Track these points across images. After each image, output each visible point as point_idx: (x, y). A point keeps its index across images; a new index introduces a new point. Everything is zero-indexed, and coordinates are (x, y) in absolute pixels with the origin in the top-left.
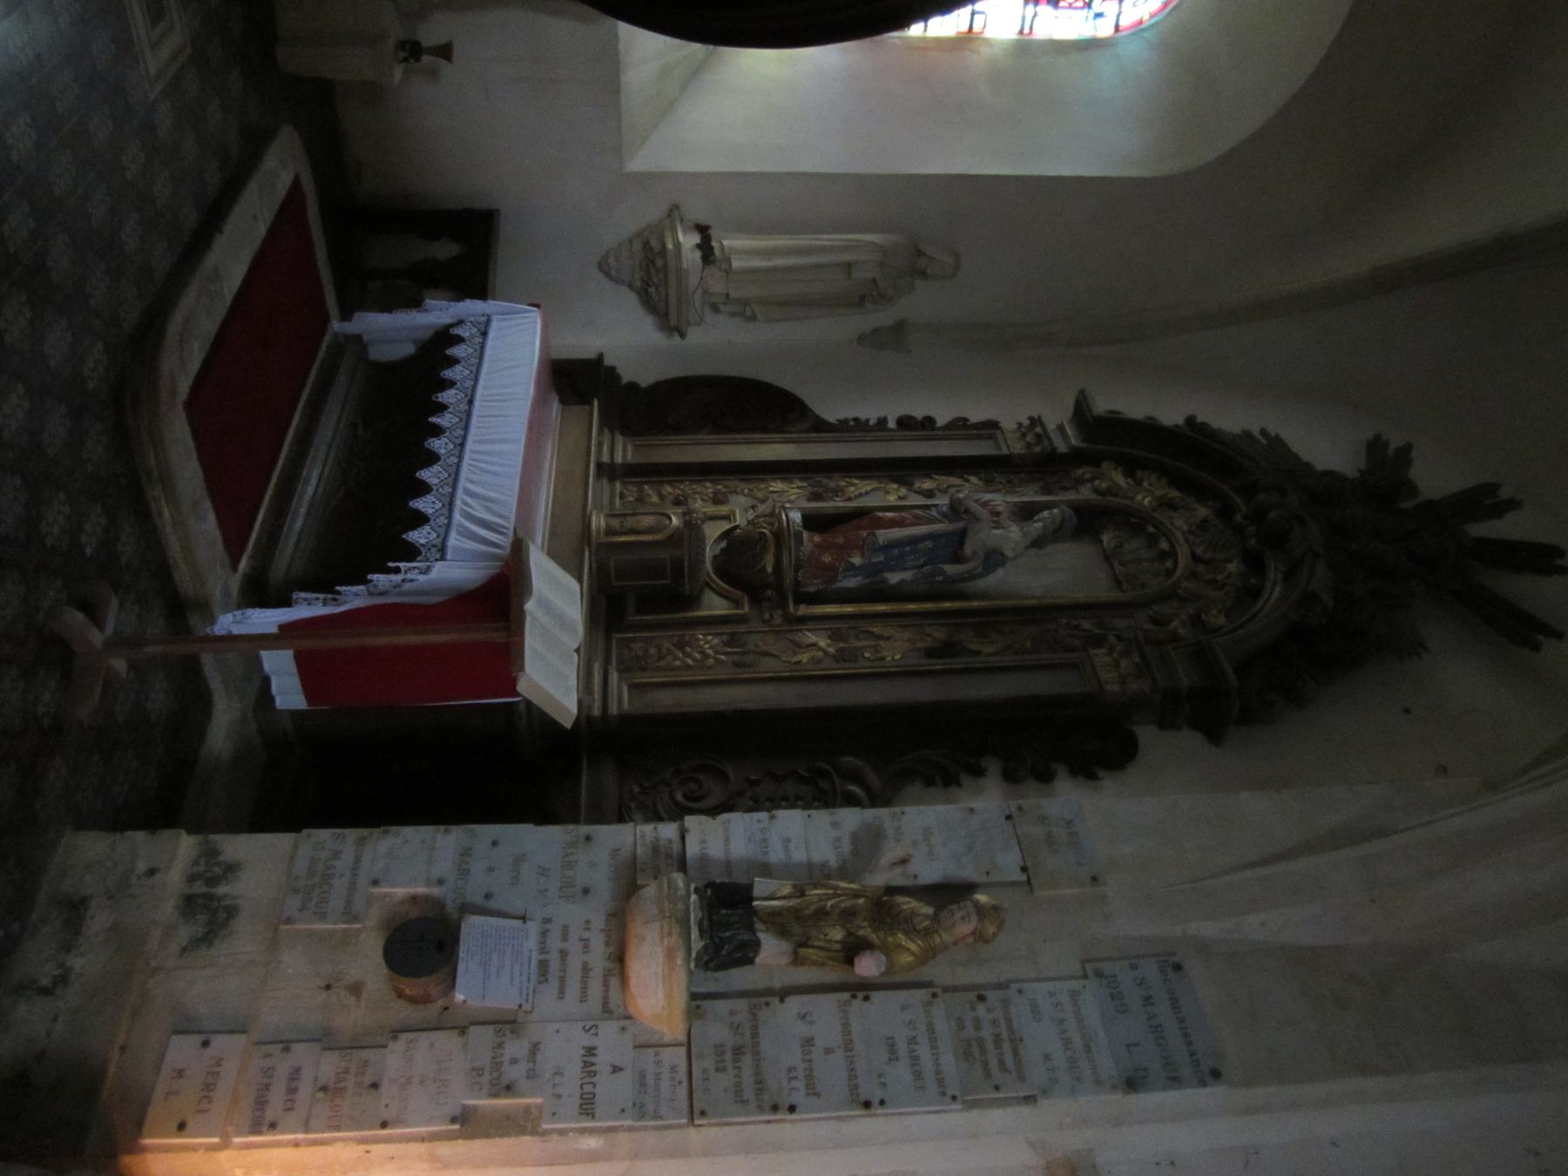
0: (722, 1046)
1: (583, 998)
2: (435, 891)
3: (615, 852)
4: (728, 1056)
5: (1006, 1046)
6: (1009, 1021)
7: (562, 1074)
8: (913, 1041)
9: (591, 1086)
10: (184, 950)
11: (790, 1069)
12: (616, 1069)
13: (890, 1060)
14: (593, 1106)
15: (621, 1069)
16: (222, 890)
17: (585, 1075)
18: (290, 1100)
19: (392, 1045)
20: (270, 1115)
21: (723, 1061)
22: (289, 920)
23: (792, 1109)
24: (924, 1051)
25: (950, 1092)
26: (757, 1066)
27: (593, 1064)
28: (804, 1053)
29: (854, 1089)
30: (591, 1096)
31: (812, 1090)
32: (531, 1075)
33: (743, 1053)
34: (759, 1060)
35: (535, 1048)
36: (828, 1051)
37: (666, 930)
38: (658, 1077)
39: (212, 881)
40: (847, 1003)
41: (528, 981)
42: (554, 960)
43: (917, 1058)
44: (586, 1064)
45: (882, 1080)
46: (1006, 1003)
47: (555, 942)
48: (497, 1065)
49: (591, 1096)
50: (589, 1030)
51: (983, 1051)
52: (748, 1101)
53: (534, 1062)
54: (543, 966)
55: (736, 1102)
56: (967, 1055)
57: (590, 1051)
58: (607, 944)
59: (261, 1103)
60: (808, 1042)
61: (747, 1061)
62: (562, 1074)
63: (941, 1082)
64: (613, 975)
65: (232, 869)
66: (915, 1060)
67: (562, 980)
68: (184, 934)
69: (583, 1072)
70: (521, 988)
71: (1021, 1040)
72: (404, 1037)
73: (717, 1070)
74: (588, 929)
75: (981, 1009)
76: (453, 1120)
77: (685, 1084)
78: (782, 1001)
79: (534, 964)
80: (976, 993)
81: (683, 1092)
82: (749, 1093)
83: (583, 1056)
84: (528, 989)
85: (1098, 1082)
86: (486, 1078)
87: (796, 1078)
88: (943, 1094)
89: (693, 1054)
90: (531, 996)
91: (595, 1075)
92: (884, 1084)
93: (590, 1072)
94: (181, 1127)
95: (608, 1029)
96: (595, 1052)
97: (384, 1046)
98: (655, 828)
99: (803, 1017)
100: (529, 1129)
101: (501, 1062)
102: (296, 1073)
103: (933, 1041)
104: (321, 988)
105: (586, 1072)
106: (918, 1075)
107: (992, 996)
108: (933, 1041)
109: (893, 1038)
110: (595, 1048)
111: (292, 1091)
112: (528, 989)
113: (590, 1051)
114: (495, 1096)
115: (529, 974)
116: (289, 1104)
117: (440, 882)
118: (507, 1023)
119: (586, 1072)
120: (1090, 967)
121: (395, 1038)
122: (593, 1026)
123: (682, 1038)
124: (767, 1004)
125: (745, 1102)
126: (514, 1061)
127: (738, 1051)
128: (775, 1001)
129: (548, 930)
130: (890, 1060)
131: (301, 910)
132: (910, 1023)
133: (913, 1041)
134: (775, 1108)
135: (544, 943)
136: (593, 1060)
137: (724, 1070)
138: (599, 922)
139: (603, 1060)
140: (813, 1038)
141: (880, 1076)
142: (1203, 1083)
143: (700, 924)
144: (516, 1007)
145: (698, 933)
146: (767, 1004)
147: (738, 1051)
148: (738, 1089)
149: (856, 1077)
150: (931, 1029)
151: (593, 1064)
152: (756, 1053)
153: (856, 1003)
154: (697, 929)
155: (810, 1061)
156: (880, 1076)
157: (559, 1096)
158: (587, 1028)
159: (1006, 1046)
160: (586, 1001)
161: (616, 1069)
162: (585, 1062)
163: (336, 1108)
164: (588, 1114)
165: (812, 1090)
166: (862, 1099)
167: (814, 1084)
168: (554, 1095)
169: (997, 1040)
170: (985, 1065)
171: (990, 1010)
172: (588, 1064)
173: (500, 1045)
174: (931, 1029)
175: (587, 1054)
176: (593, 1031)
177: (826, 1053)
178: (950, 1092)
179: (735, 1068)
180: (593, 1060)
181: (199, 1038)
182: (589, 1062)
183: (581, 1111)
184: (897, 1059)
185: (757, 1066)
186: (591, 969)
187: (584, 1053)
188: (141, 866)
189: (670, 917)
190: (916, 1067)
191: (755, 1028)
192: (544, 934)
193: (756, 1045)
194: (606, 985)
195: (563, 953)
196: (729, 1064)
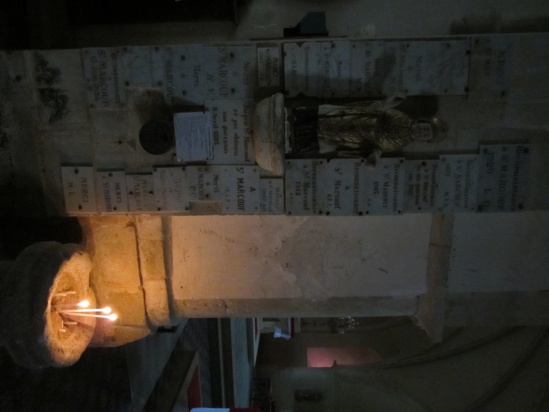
0: (299, 183)
1: (236, 153)
2: (158, 89)
3: (247, 65)
4: (302, 188)
5: (429, 190)
6: (434, 176)
7: (229, 191)
8: (386, 184)
9: (242, 197)
10: (50, 120)
11: (329, 196)
12: (253, 189)
13: (375, 193)
14: (243, 206)
15: (255, 190)
16: (55, 86)
17: (239, 191)
18: (119, 198)
19: (154, 173)
20: (114, 203)
21: (299, 190)
22: (92, 106)
23: (328, 213)
24: (391, 189)
25: (399, 208)
26: (314, 192)
27: (243, 187)
28: (336, 188)
29: (356, 206)
30: (242, 201)
31: (337, 205)
32: (216, 191)
33: (309, 187)
34: (315, 190)
35: (216, 178)
36: (347, 188)
37: (272, 149)
38: (271, 193)
39: (49, 81)
40: (358, 164)
41: (210, 145)
42: (220, 131)
43: (387, 193)
44: (240, 187)
45: (369, 202)
46: (435, 167)
47: (220, 122)
48: (201, 186)
49: (242, 201)
50: (240, 170)
51: (418, 189)
52: (309, 209)
53: (217, 184)
54: (216, 134)
55: (305, 209)
56: (410, 192)
57: (241, 180)
58: (246, 124)
59: (108, 199)
60: (338, 183)
61: (310, 190)
62: (229, 191)
63: (395, 205)
64: (249, 141)
65: (55, 73)
66: (386, 193)
67: (225, 142)
68: (48, 112)
69: (238, 190)
70: (207, 149)
71: (437, 186)
72: (159, 169)
73: (296, 194)
74: (236, 114)
75: (422, 169)
76: (187, 209)
77: (282, 197)
78: (328, 161)
79: (211, 134)
80: (422, 161)
81: (281, 201)
82: (310, 204)
83: (238, 183)
84: (210, 148)
85: (466, 207)
86: (197, 192)
87: (331, 200)
88: (395, 210)
89: (286, 186)
90: (212, 153)
91: (243, 192)
92: (370, 204)
93: (241, 190)
94: (80, 207)
95: (248, 170)
96: (243, 181)
97: (151, 174)
98: (268, 50)
99: (337, 170)
100: (218, 211)
101: (203, 184)
102: (117, 186)
103: (396, 184)
104: (117, 142)
105: (239, 190)
106: (386, 201)
107: (429, 162)
108: (396, 184)
109: (378, 183)
110: (243, 179)
111: (119, 194)
112: (210, 148)
113: (241, 180)
114: (202, 199)
115: (210, 141)
116: (119, 199)
117: (160, 84)
118: (202, 165)
119: (239, 190)
120: (482, 147)
121: (155, 170)
122: (241, 168)
123: (283, 176)
124: (321, 163)
125: (308, 209)
126: (208, 184)
127: (306, 185)
128: (325, 161)
129: (216, 115)
130: (375, 193)
131: (96, 100)
132: (387, 175)
133: (386, 184)
134: (321, 213)
135: (215, 122)
136: (242, 184)
137: (299, 194)
138: (241, 110)
139: (247, 185)
140: (340, 181)
141: (369, 200)
142: (513, 210)
143: (290, 139)
144: (206, 159)
145: (289, 144)
146: (321, 163)
147: (306, 185)
148: (305, 205)
149: (357, 201)
150: (396, 178)
151: (243, 187)
152: (314, 187)
153: (363, 164)
154: (288, 142)
155: (338, 192)
156: (369, 200)
157: (229, 201)
158: (238, 169)
159: (429, 190)
160: (237, 154)
161: (253, 189)
162: (239, 186)
163: (139, 202)
164: (241, 209)
165: (337, 205)
166: (359, 211)
167: (339, 203)
168: (227, 200)
169: (426, 185)
170: (417, 197)
171: (426, 171)
172: (240, 187)
173: (201, 176)
174: (396, 178)
175: (239, 182)
176: (241, 171)
177: (346, 189)
178: (399, 208)
179: (305, 193)
180: (242, 184)
181: (72, 169)
182: (241, 186)
183: (239, 208)
184: (378, 193)
185: (314, 192)
186: (239, 138)
187: (238, 181)
188: (13, 75)
189: (274, 143)
190: (385, 197)
191: (314, 174)
192: (214, 116)
193: (314, 183)
194: (246, 146)
195: (225, 128)
196: (302, 192)
